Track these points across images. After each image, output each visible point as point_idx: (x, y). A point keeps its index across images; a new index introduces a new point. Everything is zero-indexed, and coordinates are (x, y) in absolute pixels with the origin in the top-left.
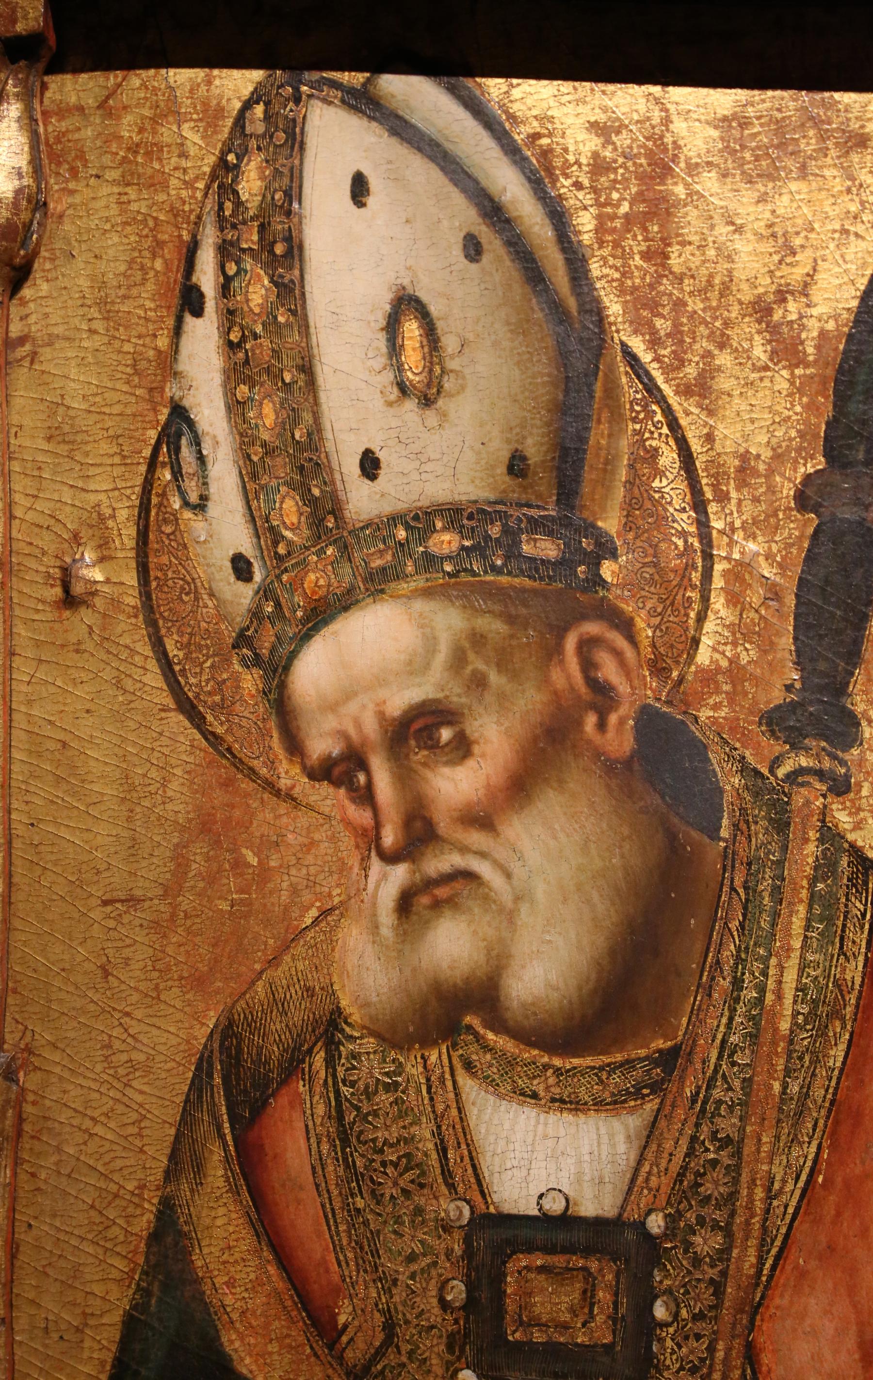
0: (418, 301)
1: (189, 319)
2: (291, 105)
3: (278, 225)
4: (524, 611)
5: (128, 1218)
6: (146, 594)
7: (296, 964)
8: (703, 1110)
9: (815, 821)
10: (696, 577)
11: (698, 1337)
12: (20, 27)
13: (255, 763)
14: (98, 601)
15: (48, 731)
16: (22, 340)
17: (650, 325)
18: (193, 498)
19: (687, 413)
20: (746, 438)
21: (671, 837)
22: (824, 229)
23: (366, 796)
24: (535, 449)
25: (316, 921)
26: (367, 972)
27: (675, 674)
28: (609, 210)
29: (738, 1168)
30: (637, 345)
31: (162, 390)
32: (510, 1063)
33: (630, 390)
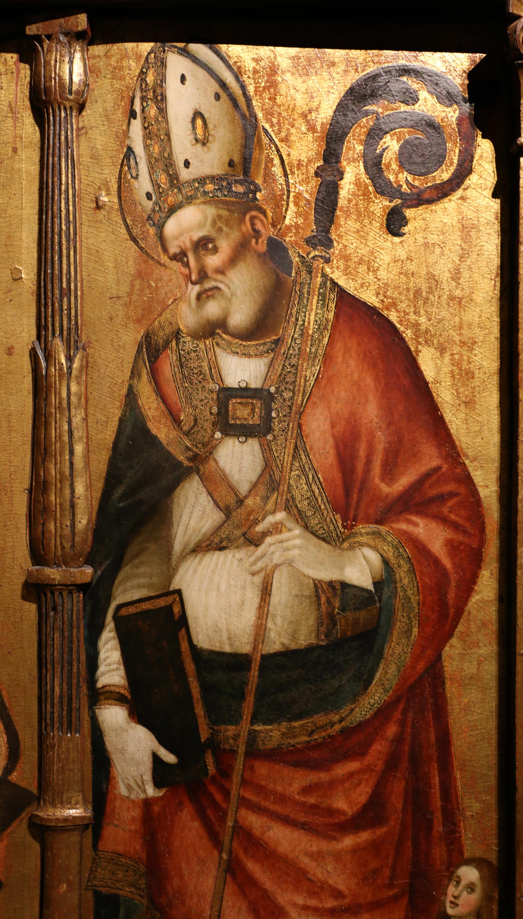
0: (201, 113)
1: (132, 120)
2: (162, 53)
3: (159, 91)
4: (233, 208)
5: (120, 390)
6: (121, 205)
7: (167, 315)
8: (287, 357)
9: (320, 271)
10: (285, 197)
11: (284, 421)
12: (80, 29)
13: (154, 256)
14: (107, 207)
15: (93, 247)
16: (83, 128)
17: (271, 120)
18: (134, 175)
19: (282, 147)
20: (300, 155)
21: (277, 275)
22: (323, 91)
23: (187, 265)
24: (236, 158)
25: (172, 303)
26: (187, 317)
27: (279, 227)
28: (258, 85)
29: (296, 373)
30: (267, 126)
31: (125, 142)
32: (230, 344)
33: (265, 140)
